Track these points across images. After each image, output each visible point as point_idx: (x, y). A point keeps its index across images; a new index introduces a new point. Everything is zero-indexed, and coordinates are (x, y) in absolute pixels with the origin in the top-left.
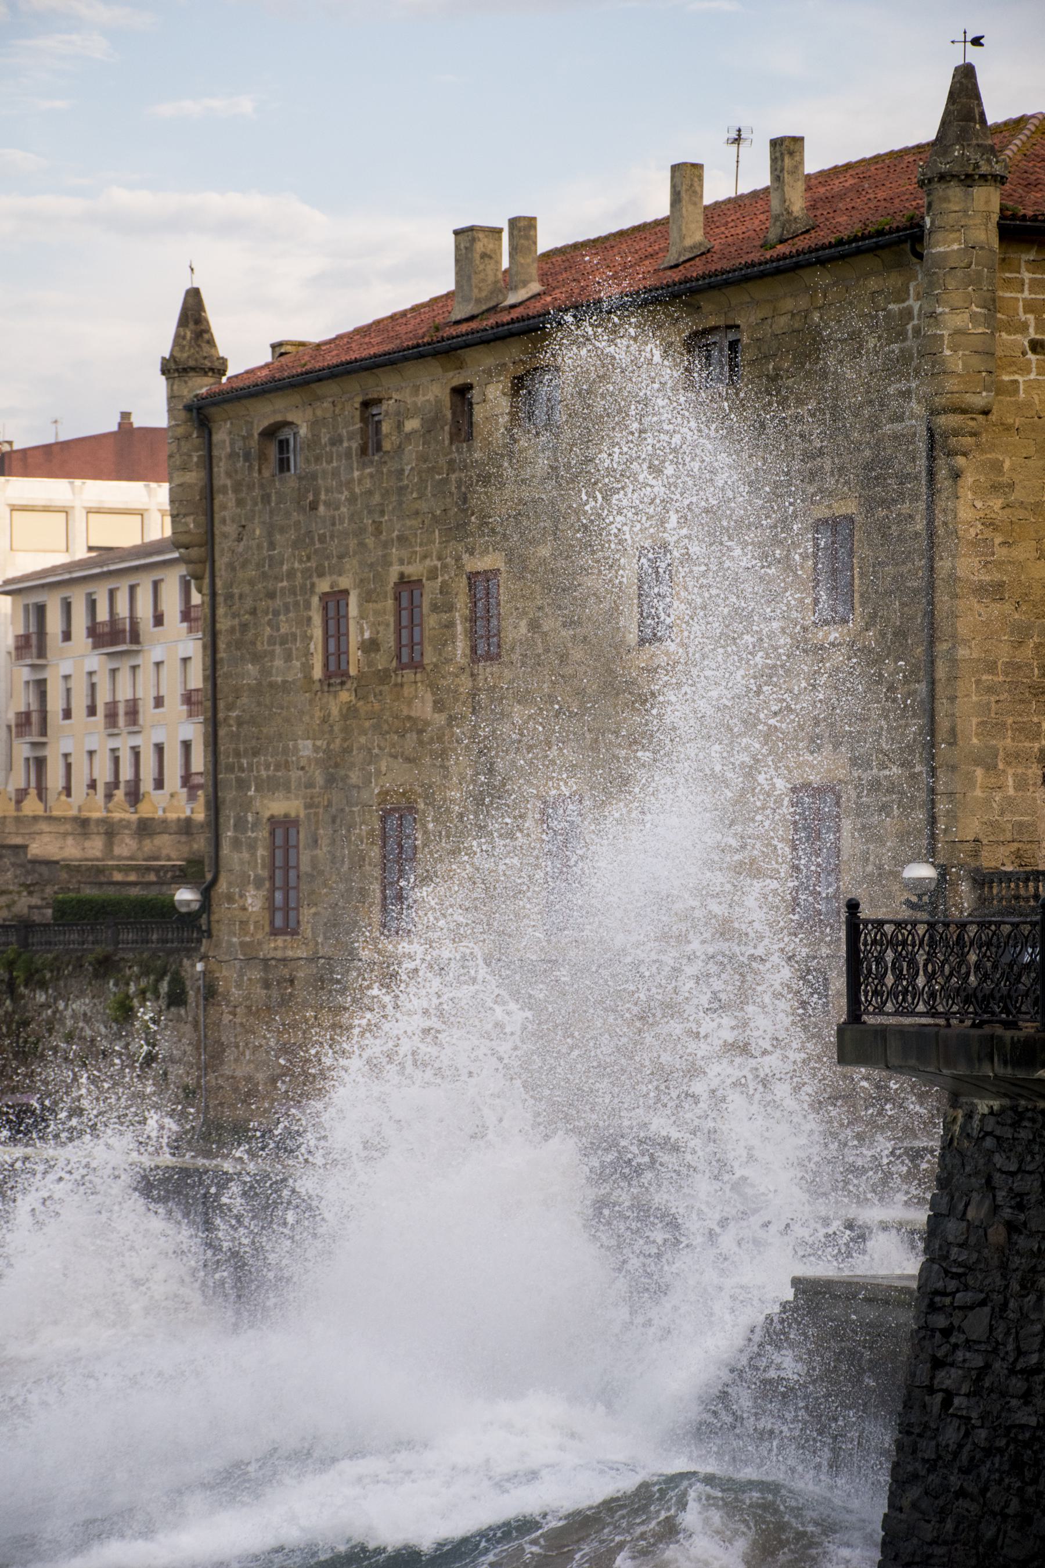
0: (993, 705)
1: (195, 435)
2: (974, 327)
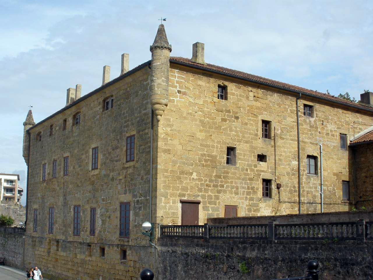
0: (167, 181)
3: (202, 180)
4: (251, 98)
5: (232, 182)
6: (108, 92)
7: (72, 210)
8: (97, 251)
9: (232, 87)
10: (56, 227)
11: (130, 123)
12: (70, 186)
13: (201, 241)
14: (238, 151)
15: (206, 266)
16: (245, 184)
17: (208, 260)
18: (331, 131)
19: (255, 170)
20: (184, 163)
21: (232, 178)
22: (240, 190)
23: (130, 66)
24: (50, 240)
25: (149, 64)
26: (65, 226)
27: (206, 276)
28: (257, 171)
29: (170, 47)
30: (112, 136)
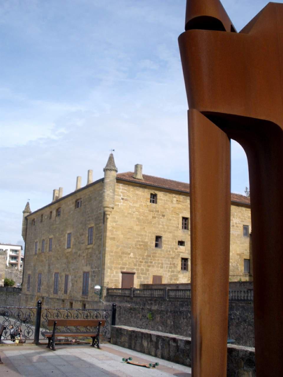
3: (137, 258)
4: (175, 202)
5: (158, 260)
6: (78, 196)
7: (53, 276)
8: (68, 305)
9: (161, 195)
10: (42, 287)
11: (91, 218)
12: (53, 259)
13: (128, 299)
14: (163, 239)
15: (131, 315)
16: (168, 261)
17: (131, 311)
18: (236, 223)
19: (176, 252)
20: (124, 247)
21: (159, 257)
22: (164, 265)
23: (93, 180)
24: (38, 297)
25: (102, 180)
26: (48, 287)
27: (130, 322)
28: (178, 252)
29: (116, 169)
30: (80, 226)
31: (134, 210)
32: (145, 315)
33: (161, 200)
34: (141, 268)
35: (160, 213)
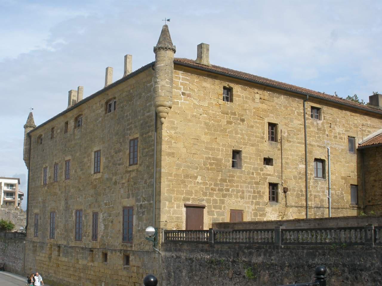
0: (171, 185)
1: (28, 139)
2: (167, 85)
3: (207, 184)
4: (257, 100)
5: (237, 186)
6: (110, 94)
7: (74, 214)
8: (99, 256)
9: (237, 89)
10: (57, 231)
11: (133, 125)
12: (72, 190)
13: (206, 247)
14: (243, 155)
15: (211, 272)
16: (251, 188)
18: (339, 134)
19: (261, 174)
20: (188, 167)
21: (238, 182)
22: (245, 194)
23: (133, 68)
24: (51, 245)
25: (152, 66)
26: (66, 231)
28: (263, 174)
31: (201, 110)
32: (240, 272)
33: (239, 96)
34: (214, 198)
35: (237, 116)
